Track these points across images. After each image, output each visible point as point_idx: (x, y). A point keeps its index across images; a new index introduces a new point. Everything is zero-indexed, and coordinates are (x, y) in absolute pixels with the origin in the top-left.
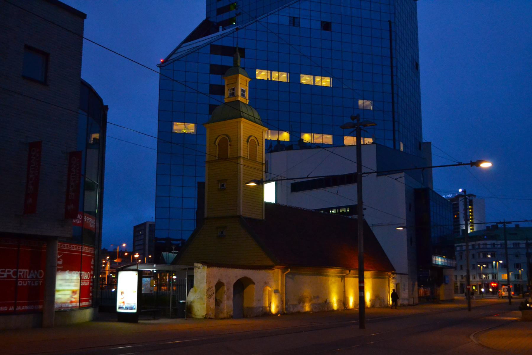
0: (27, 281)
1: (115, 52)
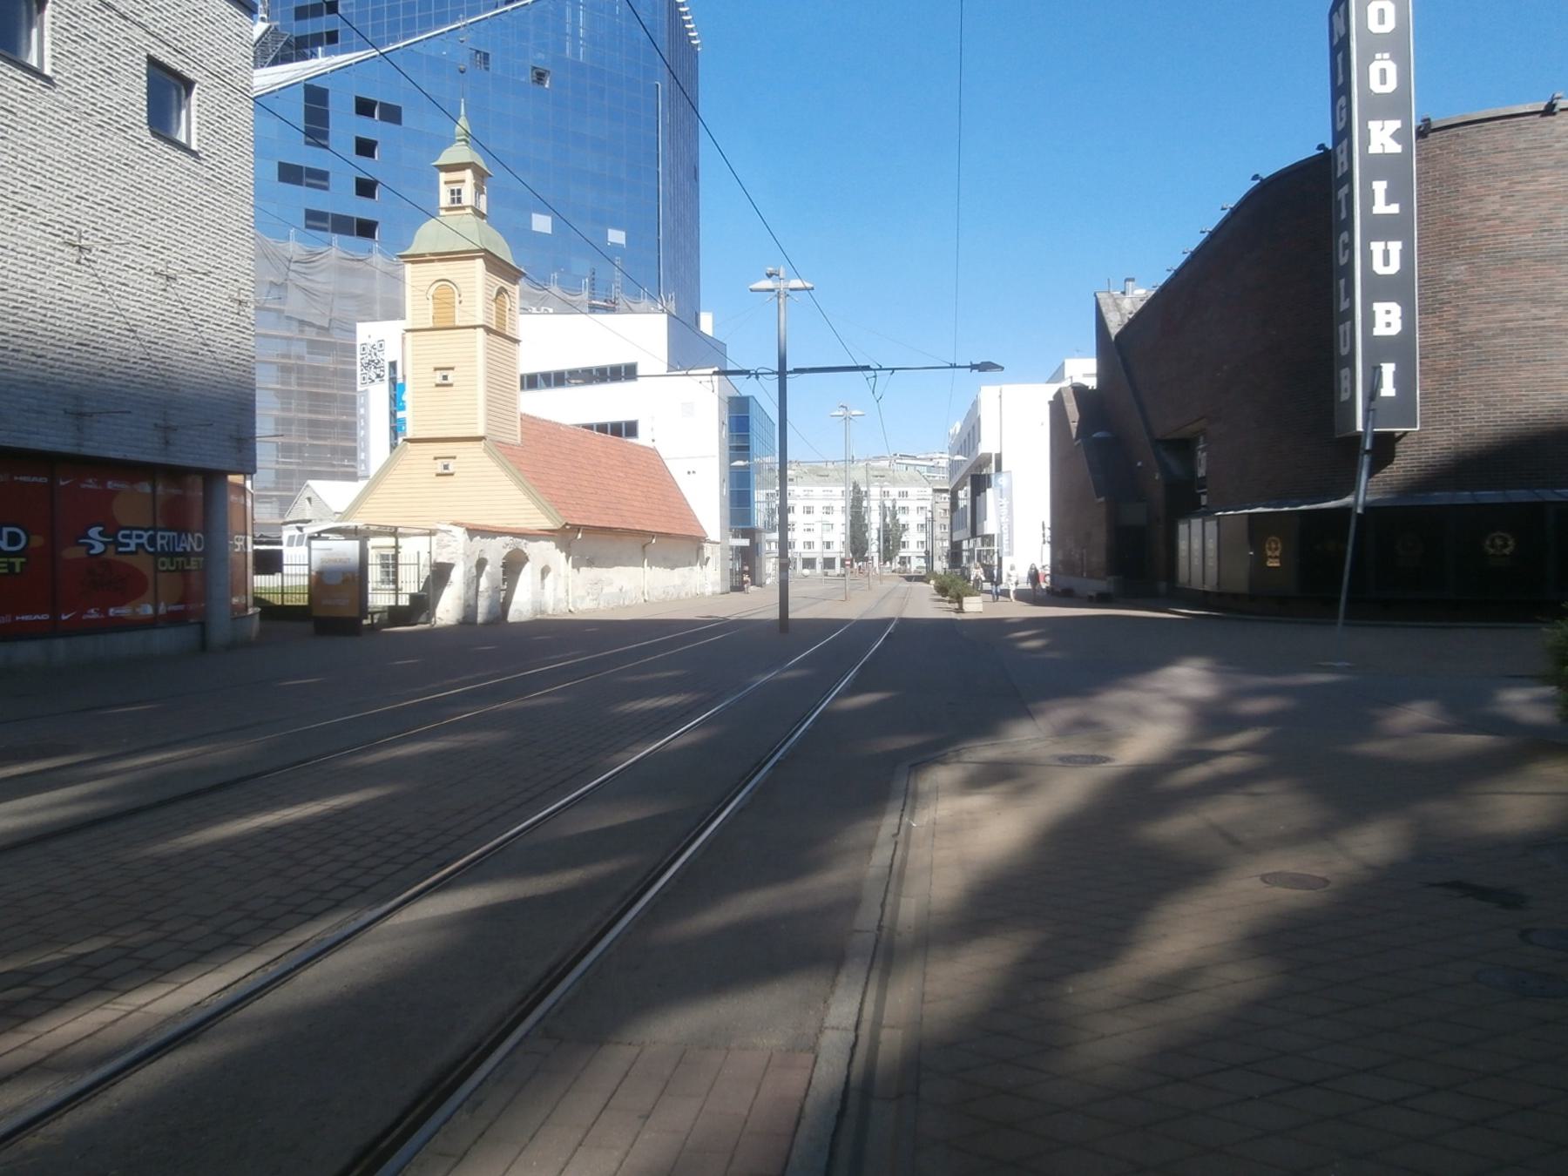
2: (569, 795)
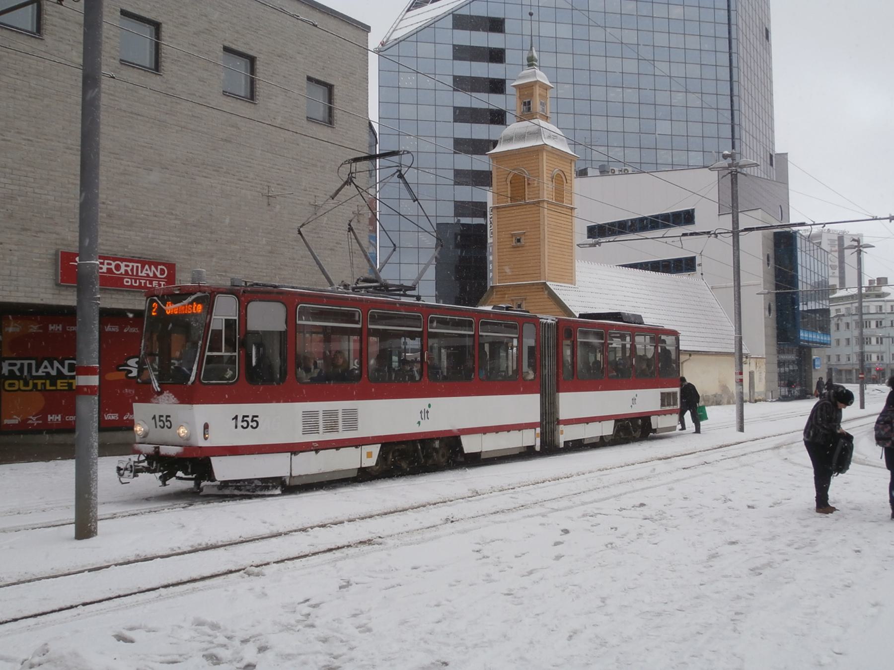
0: (139, 279)
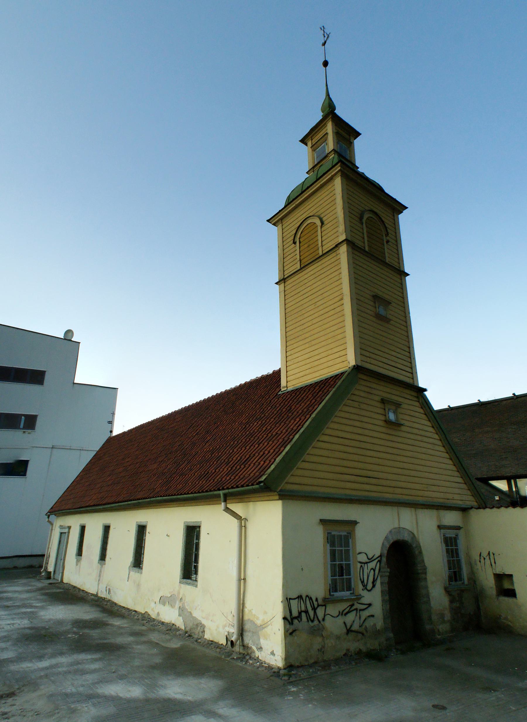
1: (387, 364)
2: (305, 198)
